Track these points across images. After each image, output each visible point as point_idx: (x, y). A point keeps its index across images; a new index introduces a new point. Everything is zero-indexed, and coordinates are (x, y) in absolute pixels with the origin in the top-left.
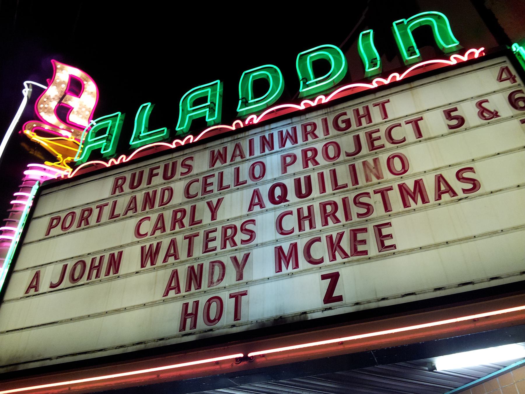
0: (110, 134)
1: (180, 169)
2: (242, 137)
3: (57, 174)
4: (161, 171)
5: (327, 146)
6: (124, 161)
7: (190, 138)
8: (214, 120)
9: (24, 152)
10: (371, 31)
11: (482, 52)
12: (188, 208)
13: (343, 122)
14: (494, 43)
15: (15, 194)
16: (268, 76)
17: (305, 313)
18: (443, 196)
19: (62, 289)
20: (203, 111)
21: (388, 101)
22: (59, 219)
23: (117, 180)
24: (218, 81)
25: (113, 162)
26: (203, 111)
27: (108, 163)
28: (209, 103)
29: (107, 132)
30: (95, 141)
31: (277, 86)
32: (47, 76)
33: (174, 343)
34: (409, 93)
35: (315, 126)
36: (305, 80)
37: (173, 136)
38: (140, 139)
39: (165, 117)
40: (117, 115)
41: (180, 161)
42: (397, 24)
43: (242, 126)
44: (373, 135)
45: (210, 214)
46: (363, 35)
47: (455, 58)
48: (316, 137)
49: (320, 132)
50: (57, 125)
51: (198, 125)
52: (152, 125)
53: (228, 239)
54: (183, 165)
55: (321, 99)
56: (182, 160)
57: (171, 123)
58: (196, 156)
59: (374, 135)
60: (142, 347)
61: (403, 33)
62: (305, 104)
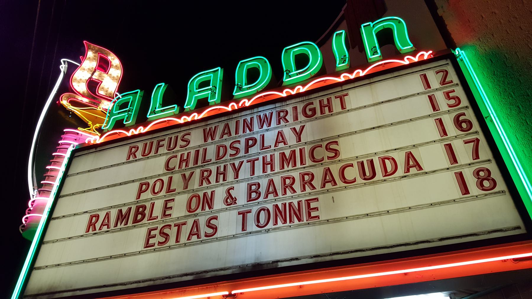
1: (180, 143)
4: (165, 143)
6: (196, 118)
8: (215, 102)
10: (344, 31)
11: (430, 54)
12: (165, 179)
13: (310, 110)
14: (442, 46)
16: (259, 67)
17: (278, 261)
18: (327, 184)
20: (205, 93)
21: (347, 95)
26: (205, 93)
30: (119, 113)
31: (316, 62)
32: (78, 55)
34: (368, 87)
36: (288, 72)
37: (182, 112)
38: (155, 114)
39: (176, 96)
40: (137, 92)
41: (180, 135)
42: (364, 26)
44: (450, 94)
45: (182, 184)
46: (337, 35)
47: (407, 59)
48: (287, 121)
49: (290, 117)
51: (202, 104)
52: (166, 102)
57: (181, 102)
58: (193, 132)
60: (151, 283)
62: (286, 92)
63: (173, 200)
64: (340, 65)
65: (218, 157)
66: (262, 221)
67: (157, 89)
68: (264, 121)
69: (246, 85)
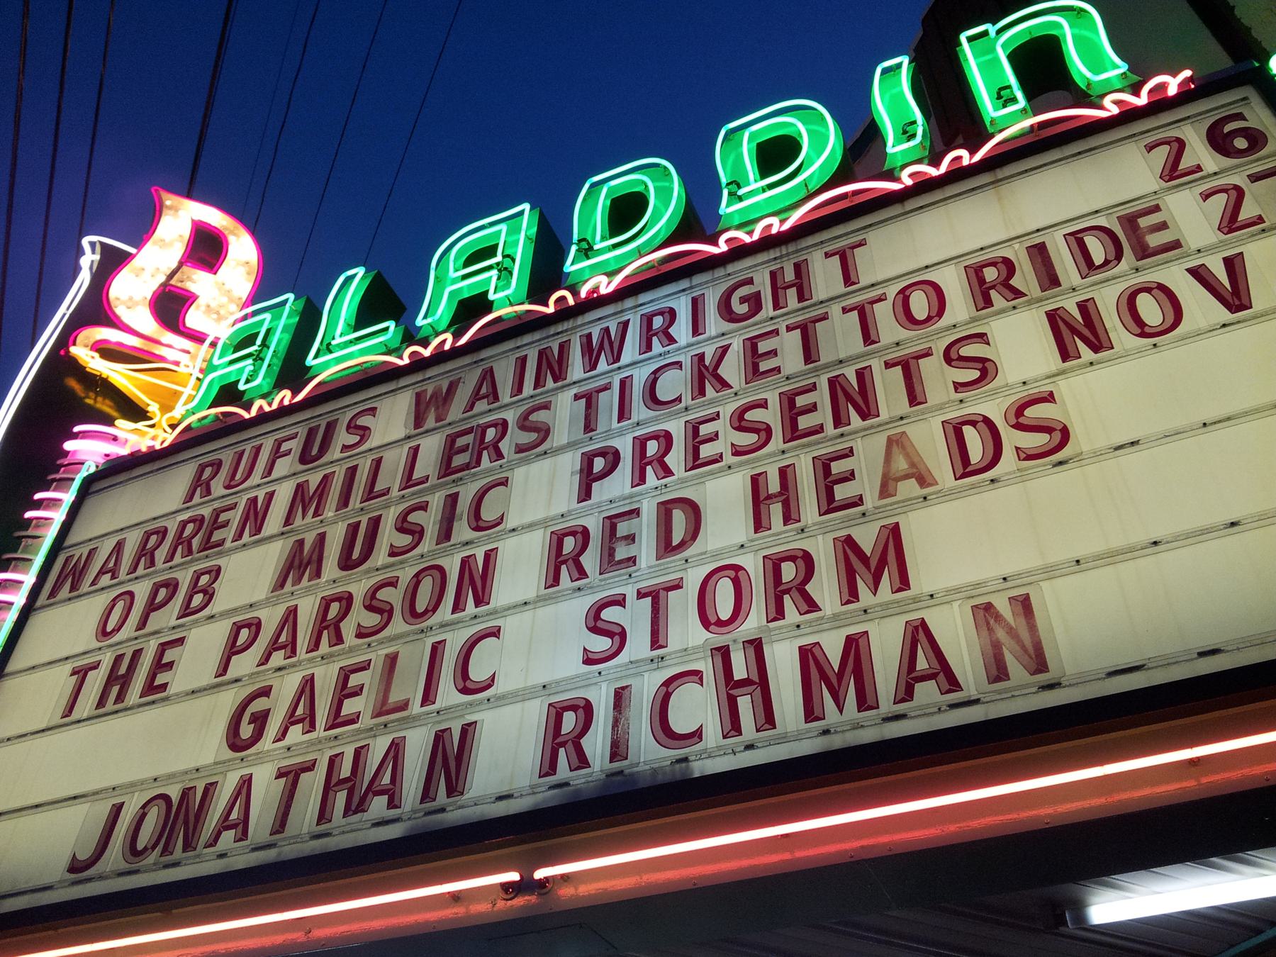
0: (264, 344)
2: (566, 331)
3: (129, 444)
4: (295, 446)
5: (907, 293)
7: (445, 341)
9: (65, 399)
10: (905, 60)
13: (743, 300)
15: (38, 496)
16: (800, 134)
19: (79, 721)
21: (861, 244)
22: (163, 533)
23: (202, 469)
24: (526, 206)
25: (261, 408)
27: (547, 306)
28: (499, 258)
29: (259, 342)
31: (822, 143)
33: (240, 866)
34: (990, 194)
35: (672, 315)
38: (331, 352)
42: (970, 39)
43: (571, 302)
49: (682, 330)
50: (155, 336)
52: (368, 313)
53: (565, 562)
54: (352, 427)
55: (960, 158)
56: (349, 415)
58: (384, 406)
59: (1143, 222)
61: (986, 60)
63: (180, 641)
64: (730, 210)
65: (447, 469)
66: (724, 605)
67: (588, 193)
68: (601, 348)
69: (603, 239)
